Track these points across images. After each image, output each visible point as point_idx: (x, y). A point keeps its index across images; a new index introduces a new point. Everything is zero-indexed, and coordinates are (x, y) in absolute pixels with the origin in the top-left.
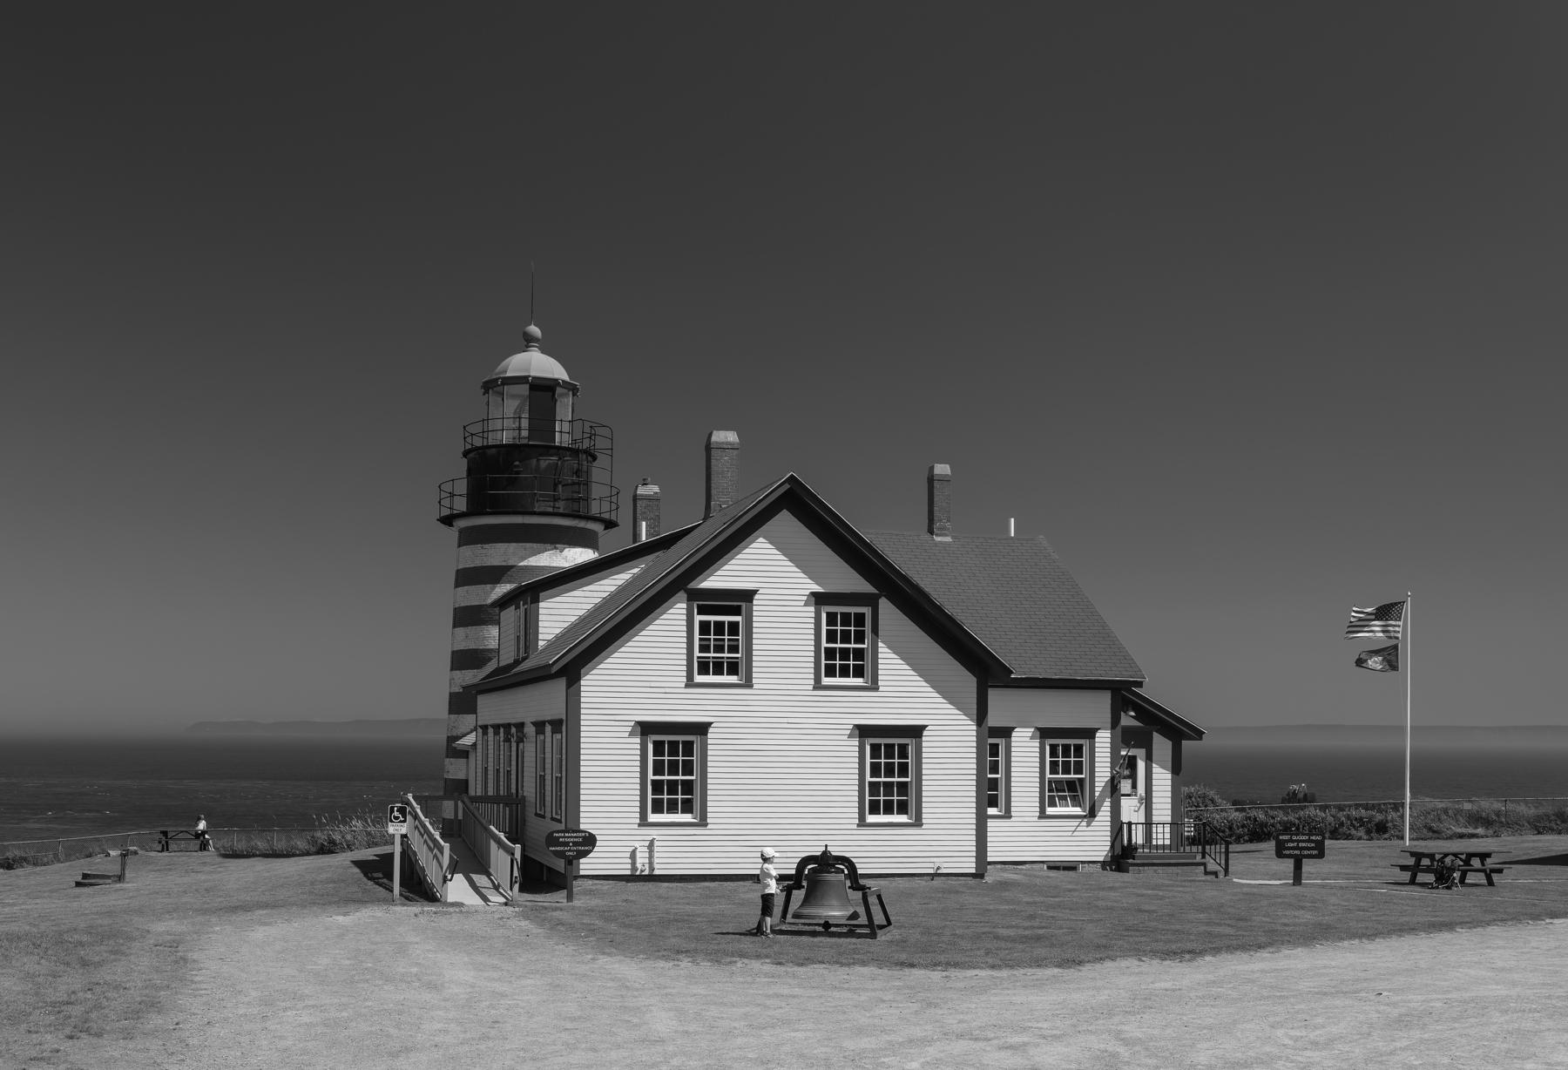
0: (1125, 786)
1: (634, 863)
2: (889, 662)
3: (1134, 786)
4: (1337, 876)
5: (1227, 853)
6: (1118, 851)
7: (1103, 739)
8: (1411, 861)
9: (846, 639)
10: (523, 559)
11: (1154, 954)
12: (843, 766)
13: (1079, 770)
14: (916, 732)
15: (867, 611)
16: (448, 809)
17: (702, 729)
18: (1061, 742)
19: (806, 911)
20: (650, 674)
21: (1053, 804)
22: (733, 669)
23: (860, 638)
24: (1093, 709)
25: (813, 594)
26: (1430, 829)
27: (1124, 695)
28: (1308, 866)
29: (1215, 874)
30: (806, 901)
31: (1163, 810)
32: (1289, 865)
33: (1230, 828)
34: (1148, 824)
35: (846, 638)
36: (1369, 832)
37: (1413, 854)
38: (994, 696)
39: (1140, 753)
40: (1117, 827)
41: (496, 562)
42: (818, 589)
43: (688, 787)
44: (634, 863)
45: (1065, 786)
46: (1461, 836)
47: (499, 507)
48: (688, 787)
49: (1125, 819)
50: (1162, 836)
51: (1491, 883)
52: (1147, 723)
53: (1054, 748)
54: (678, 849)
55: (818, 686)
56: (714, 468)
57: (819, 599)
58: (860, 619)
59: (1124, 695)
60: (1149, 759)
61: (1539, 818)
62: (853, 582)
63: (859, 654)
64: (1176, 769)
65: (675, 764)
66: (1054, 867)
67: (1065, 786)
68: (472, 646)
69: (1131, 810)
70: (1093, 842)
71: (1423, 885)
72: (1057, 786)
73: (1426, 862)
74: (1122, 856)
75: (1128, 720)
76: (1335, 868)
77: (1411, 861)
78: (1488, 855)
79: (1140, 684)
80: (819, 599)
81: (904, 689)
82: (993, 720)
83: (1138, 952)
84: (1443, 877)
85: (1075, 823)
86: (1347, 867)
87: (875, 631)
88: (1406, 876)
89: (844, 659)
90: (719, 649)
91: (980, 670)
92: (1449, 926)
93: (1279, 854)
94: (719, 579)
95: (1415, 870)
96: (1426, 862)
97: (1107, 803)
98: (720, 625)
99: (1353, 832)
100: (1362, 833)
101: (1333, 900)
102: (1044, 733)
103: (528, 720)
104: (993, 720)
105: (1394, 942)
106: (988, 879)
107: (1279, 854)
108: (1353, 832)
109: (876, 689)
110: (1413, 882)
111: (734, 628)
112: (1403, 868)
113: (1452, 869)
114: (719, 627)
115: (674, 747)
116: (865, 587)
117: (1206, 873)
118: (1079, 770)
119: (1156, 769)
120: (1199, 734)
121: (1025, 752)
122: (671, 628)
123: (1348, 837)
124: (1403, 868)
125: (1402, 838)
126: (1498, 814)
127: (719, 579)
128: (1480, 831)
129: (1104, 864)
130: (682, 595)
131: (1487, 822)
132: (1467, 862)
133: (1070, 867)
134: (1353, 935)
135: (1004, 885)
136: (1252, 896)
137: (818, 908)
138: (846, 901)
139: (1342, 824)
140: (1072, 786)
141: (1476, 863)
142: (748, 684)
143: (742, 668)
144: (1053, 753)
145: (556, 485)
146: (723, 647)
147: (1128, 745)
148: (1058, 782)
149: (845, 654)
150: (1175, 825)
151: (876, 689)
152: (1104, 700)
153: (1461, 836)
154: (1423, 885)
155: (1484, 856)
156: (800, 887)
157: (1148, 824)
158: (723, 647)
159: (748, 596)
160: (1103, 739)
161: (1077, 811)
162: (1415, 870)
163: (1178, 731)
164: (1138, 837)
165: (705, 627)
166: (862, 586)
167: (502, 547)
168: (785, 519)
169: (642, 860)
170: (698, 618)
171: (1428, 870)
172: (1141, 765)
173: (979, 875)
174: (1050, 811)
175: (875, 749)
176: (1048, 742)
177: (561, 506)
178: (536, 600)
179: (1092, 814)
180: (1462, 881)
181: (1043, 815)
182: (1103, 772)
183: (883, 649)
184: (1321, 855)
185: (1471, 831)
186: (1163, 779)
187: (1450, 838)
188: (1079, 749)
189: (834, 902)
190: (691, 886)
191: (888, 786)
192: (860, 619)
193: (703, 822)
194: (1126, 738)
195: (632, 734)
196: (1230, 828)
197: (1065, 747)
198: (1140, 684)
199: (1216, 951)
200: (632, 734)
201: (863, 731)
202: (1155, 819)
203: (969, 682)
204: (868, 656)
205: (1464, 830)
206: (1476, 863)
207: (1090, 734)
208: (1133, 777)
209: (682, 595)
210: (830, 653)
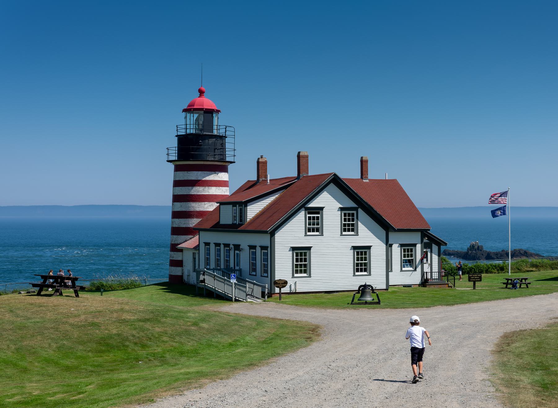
0: (425, 260)
1: (291, 289)
2: (361, 227)
3: (427, 260)
4: (486, 286)
5: (454, 279)
6: (423, 281)
7: (419, 247)
8: (506, 281)
9: (349, 221)
10: (204, 177)
11: (444, 305)
12: (349, 258)
13: (412, 256)
14: (369, 248)
15: (355, 212)
16: (254, 273)
17: (309, 248)
18: (406, 248)
19: (362, 299)
20: (292, 233)
21: (404, 267)
22: (318, 230)
23: (353, 220)
24: (415, 238)
25: (340, 208)
26: (518, 269)
27: (424, 233)
28: (477, 284)
29: (451, 287)
30: (361, 296)
31: (435, 268)
32: (472, 283)
33: (451, 270)
34: (431, 272)
35: (349, 220)
36: (498, 270)
37: (506, 279)
38: (391, 235)
39: (429, 250)
40: (423, 273)
41: (193, 178)
42: (342, 206)
43: (305, 266)
44: (291, 289)
45: (408, 261)
46: (528, 271)
47: (195, 158)
48: (305, 266)
49: (425, 271)
50: (435, 276)
51: (527, 287)
52: (431, 241)
53: (404, 250)
54: (302, 284)
55: (342, 235)
56: (301, 164)
57: (341, 209)
58: (353, 214)
59: (424, 233)
60: (431, 252)
61: (553, 264)
62: (352, 204)
63: (353, 225)
64: (439, 255)
65: (302, 258)
66: (405, 286)
67: (408, 261)
68: (184, 210)
69: (427, 268)
70: (415, 278)
71: (509, 288)
72: (406, 261)
73: (510, 281)
74: (425, 283)
75: (426, 240)
76: (486, 284)
77: (506, 281)
78: (527, 279)
79: (429, 230)
80: (341, 209)
81: (366, 235)
82: (390, 243)
83: (441, 305)
84: (514, 286)
85: (411, 272)
86: (490, 281)
87: (357, 218)
88: (505, 285)
89: (349, 226)
90: (314, 224)
91: (385, 227)
92: (509, 298)
93: (469, 281)
94: (312, 205)
95: (507, 284)
96: (510, 281)
97: (420, 266)
98: (314, 217)
99: (493, 270)
100: (496, 271)
101: (484, 293)
102: (402, 245)
103: (222, 243)
104: (390, 243)
105: (496, 301)
106: (390, 290)
107: (469, 281)
108: (493, 270)
109: (358, 235)
110: (506, 287)
111: (318, 218)
112: (504, 283)
113: (516, 283)
114: (314, 218)
115: (301, 254)
116: (354, 205)
117: (449, 287)
118: (412, 256)
119: (433, 255)
120: (446, 244)
121: (396, 250)
122: (300, 218)
123: (491, 272)
124: (504, 283)
125: (508, 272)
126: (540, 263)
127: (312, 205)
128: (534, 269)
129: (419, 285)
130: (303, 209)
131: (536, 266)
132: (521, 281)
133: (409, 286)
134: (487, 300)
135: (394, 292)
136: (462, 292)
137: (363, 297)
138: (371, 296)
139: (489, 268)
140: (409, 261)
141: (523, 281)
142: (322, 235)
143: (320, 230)
144: (404, 251)
145: (215, 149)
146: (315, 225)
147: (425, 248)
148: (405, 260)
149: (349, 225)
150: (439, 272)
151: (358, 235)
152: (419, 235)
153: (528, 271)
154: (509, 288)
155: (526, 279)
156: (359, 293)
157: (431, 272)
158: (315, 225)
159: (322, 209)
160: (419, 247)
161: (411, 269)
162: (507, 284)
163: (439, 243)
164: (429, 277)
165: (310, 218)
166: (353, 205)
167: (195, 173)
168: (332, 186)
169: (293, 287)
170: (308, 215)
171: (510, 284)
172: (429, 254)
173: (387, 289)
174: (404, 269)
175: (358, 253)
176: (403, 248)
177: (217, 158)
178: (246, 206)
179: (415, 270)
180: (520, 287)
181: (401, 271)
182: (419, 257)
183: (359, 223)
184: (481, 280)
185: (531, 269)
186: (435, 258)
187: (524, 272)
188: (412, 250)
189: (368, 296)
190: (308, 295)
191: (361, 264)
192: (353, 214)
193: (310, 276)
194: (427, 246)
195: (289, 251)
196: (451, 270)
197: (407, 249)
198: (429, 230)
199: (457, 304)
200: (289, 251)
201: (354, 248)
202: (433, 271)
203: (384, 232)
204: (355, 225)
205: (529, 269)
206: (523, 281)
207: (415, 245)
208: (427, 257)
209: (303, 209)
210: (345, 225)
